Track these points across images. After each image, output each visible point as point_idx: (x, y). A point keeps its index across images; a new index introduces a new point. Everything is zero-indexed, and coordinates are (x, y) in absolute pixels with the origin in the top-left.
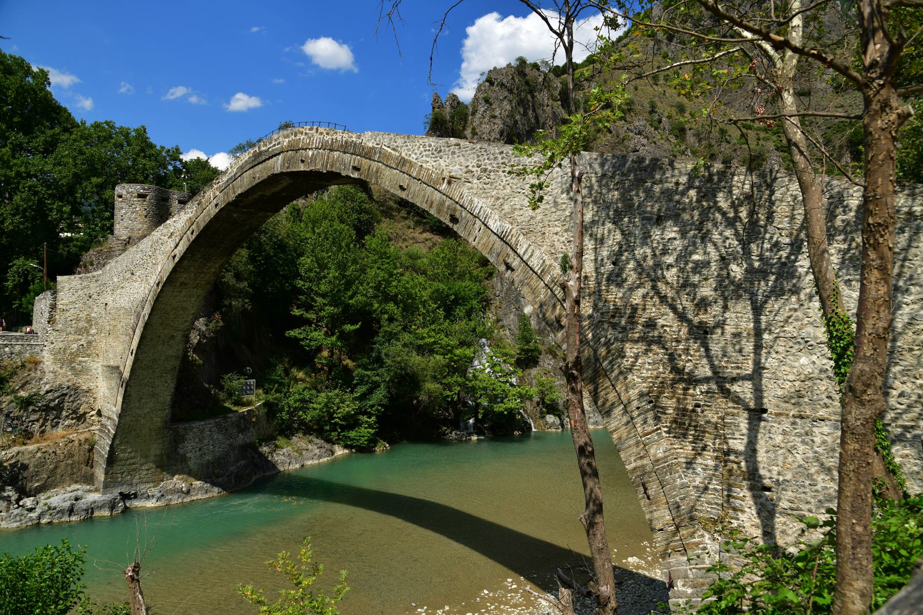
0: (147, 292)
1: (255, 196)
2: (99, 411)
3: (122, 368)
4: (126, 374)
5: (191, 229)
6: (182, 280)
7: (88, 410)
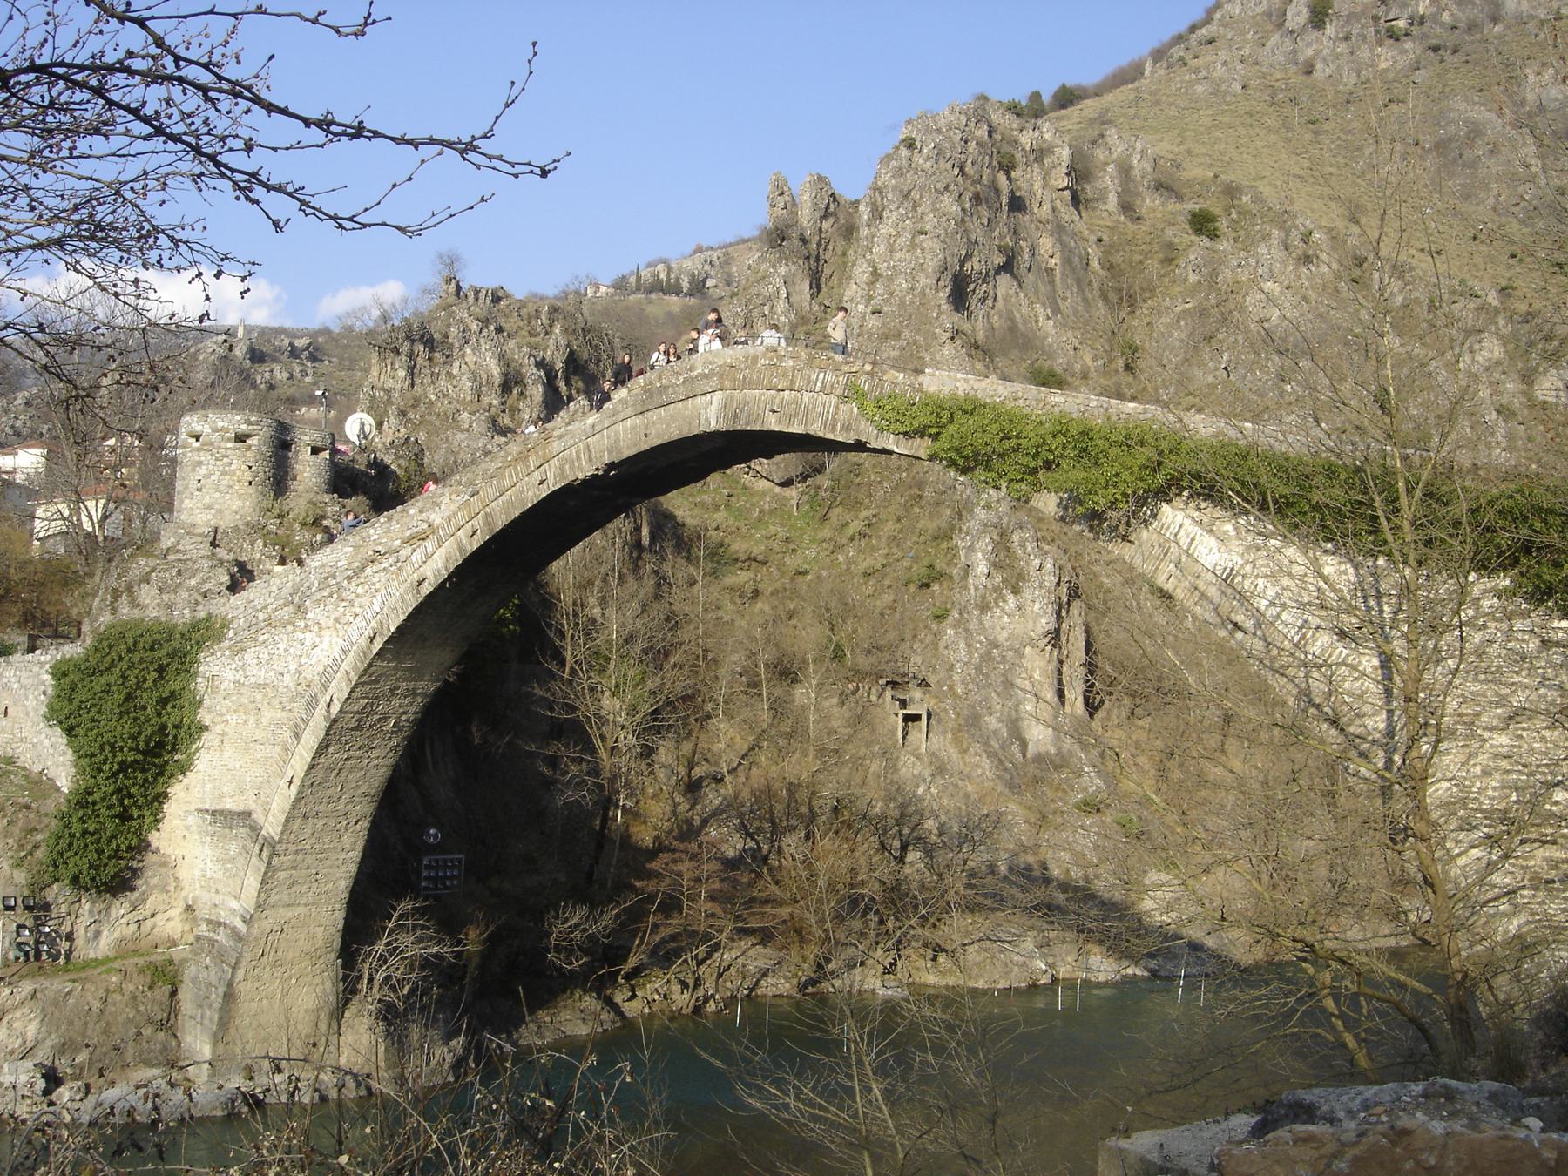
0: (337, 652)
4: (272, 826)
5: (468, 526)
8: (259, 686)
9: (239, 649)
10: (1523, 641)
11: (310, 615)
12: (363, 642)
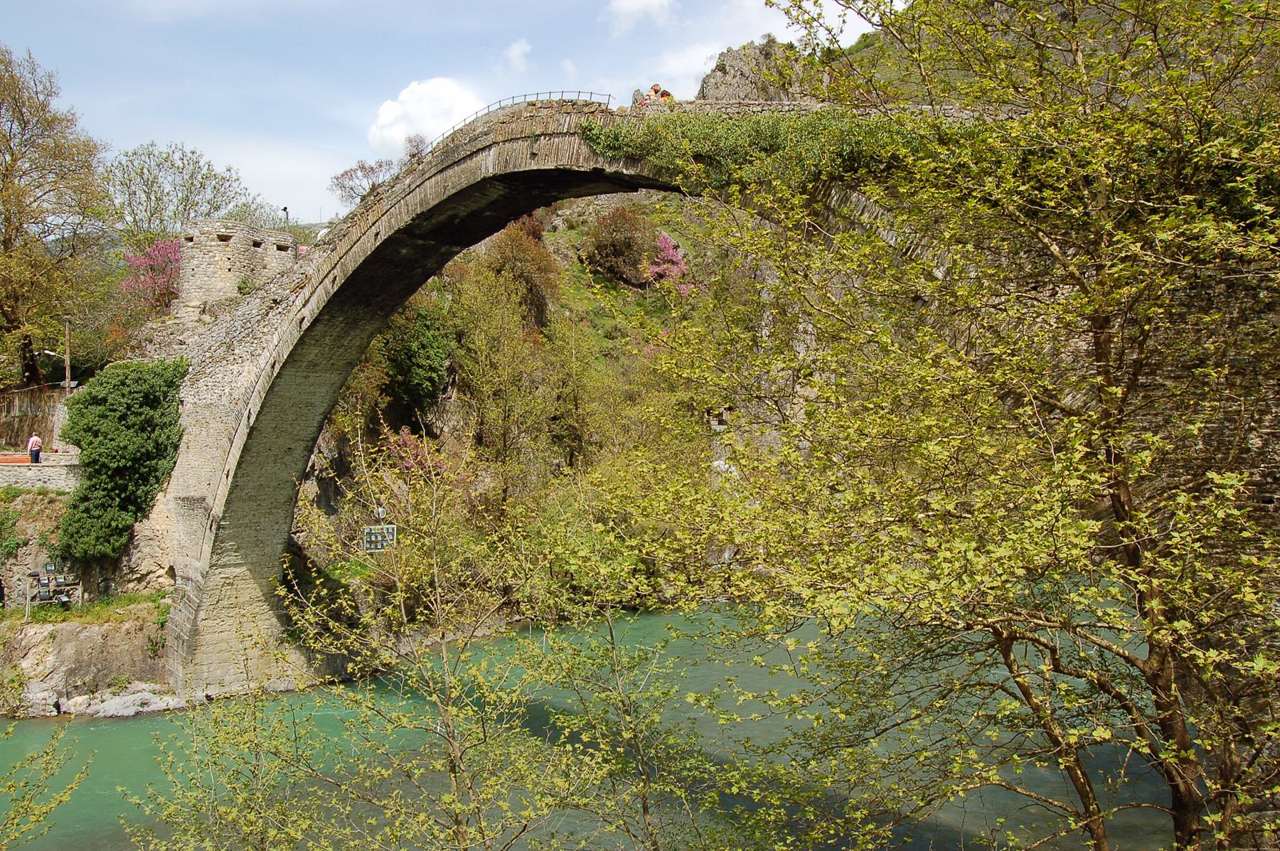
0: (253, 378)
1: (442, 218)
2: (172, 569)
3: (209, 501)
4: (218, 510)
5: (331, 276)
6: (312, 357)
7: (154, 569)
8: (208, 406)
9: (194, 382)
10: (1178, 236)
11: (236, 351)
12: (268, 368)
